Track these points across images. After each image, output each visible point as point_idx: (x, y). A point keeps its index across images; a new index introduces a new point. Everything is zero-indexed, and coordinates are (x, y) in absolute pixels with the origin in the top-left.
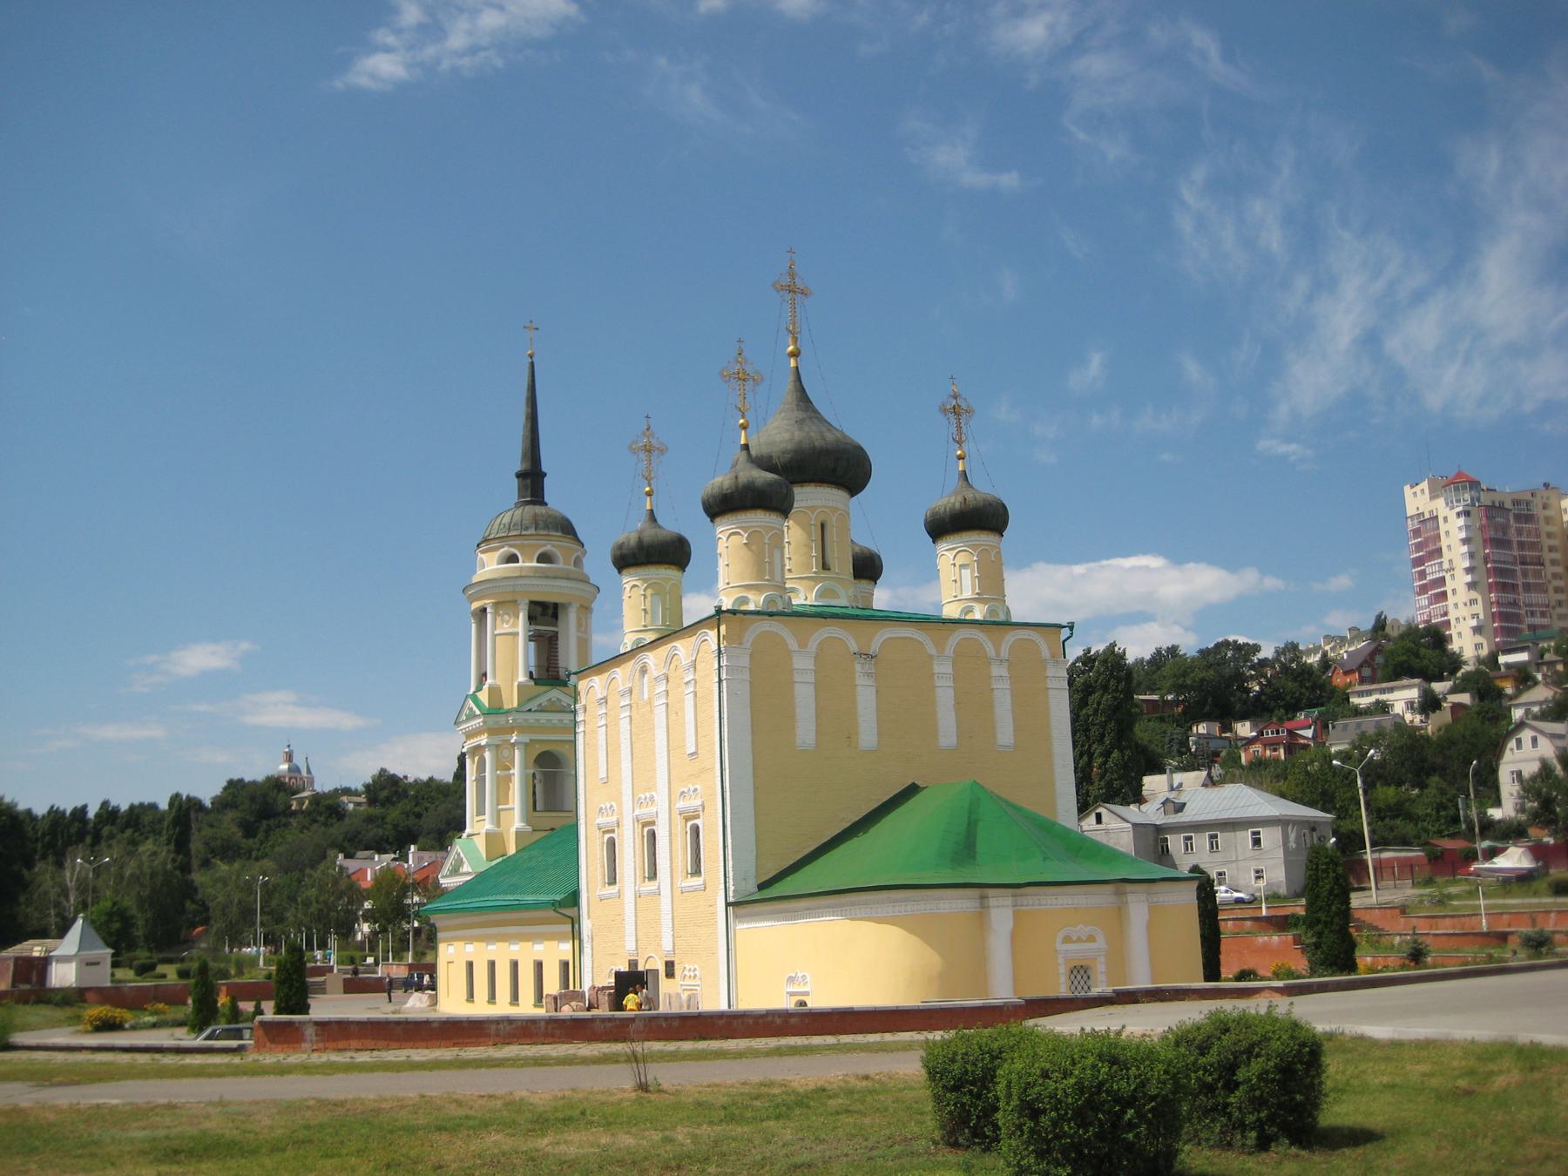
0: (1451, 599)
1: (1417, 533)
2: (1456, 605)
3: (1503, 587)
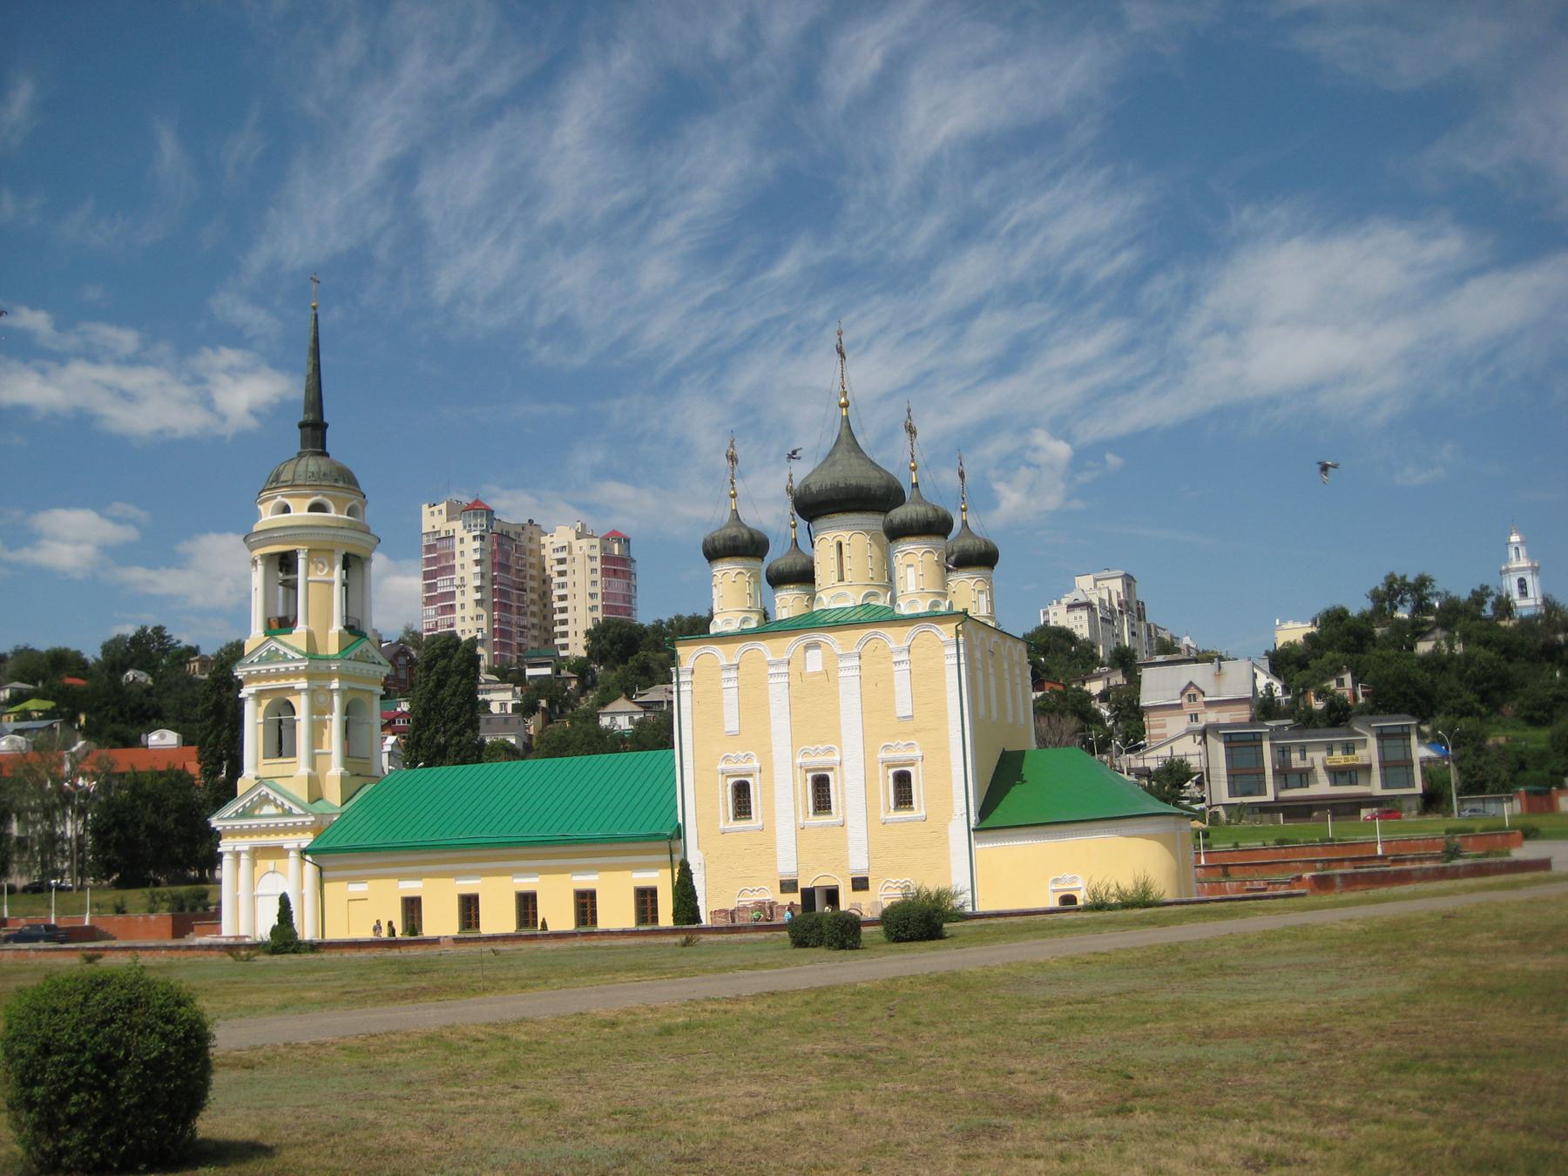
0: (459, 613)
1: (430, 548)
2: (463, 618)
3: (504, 607)
